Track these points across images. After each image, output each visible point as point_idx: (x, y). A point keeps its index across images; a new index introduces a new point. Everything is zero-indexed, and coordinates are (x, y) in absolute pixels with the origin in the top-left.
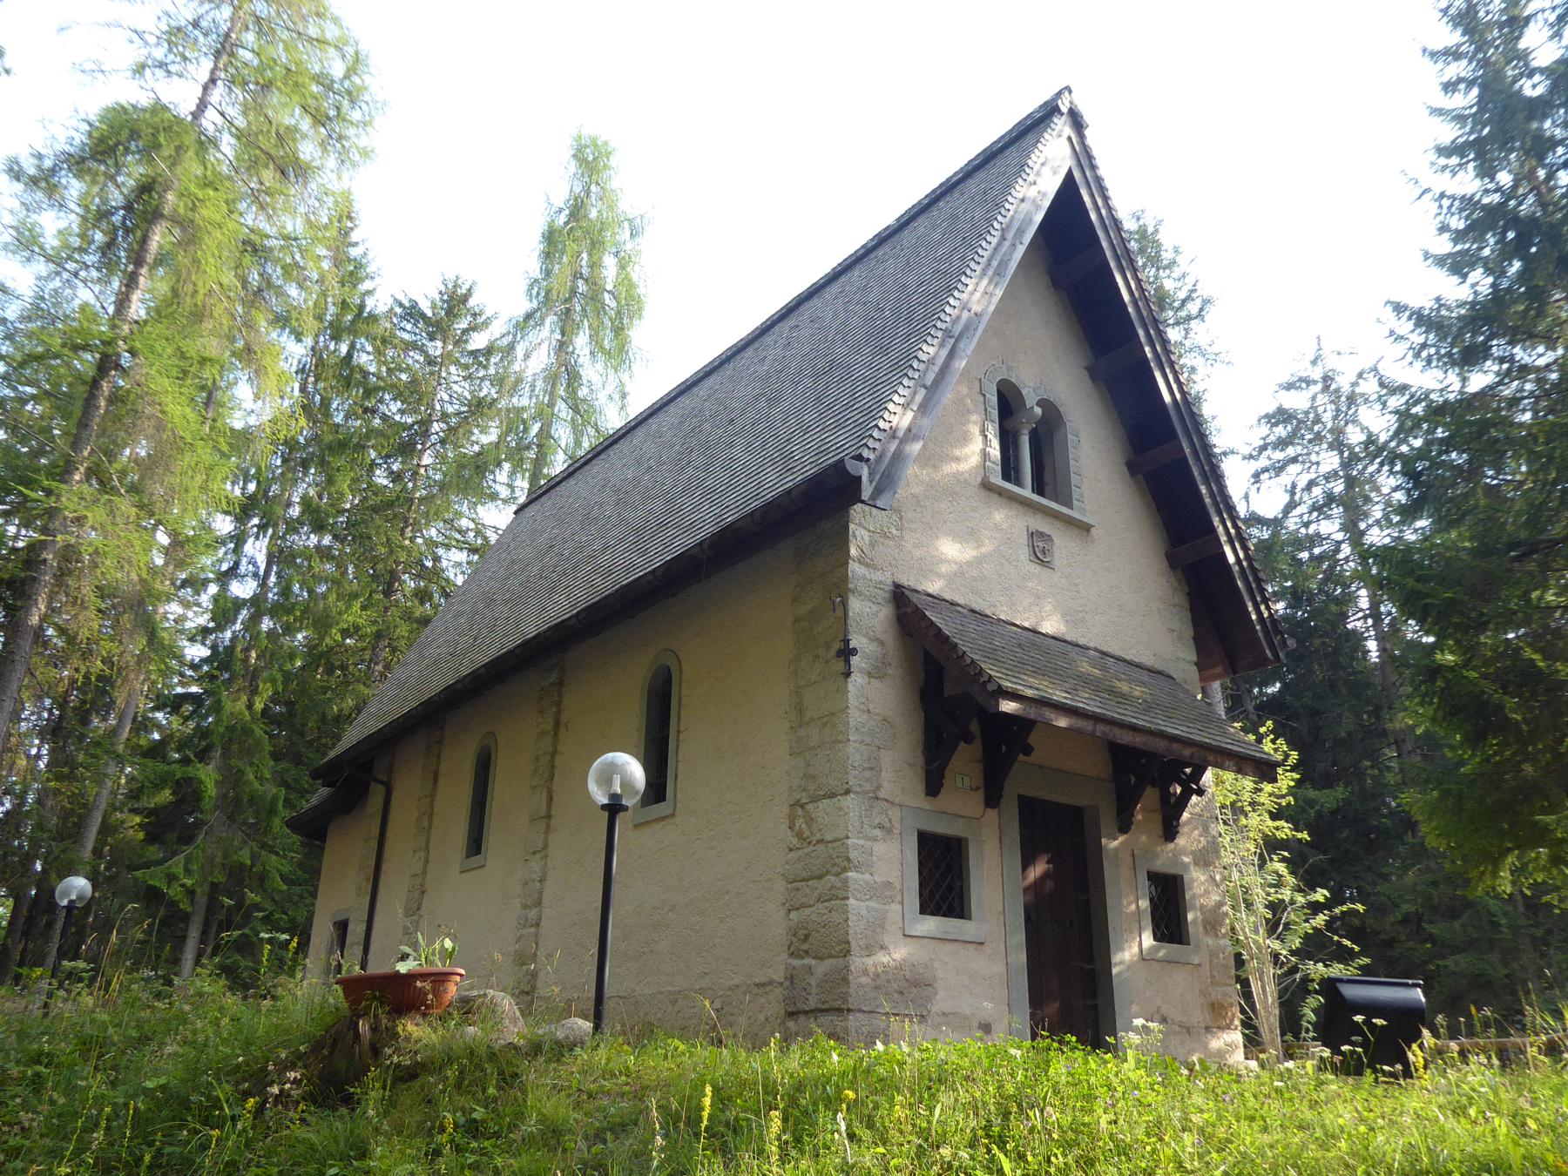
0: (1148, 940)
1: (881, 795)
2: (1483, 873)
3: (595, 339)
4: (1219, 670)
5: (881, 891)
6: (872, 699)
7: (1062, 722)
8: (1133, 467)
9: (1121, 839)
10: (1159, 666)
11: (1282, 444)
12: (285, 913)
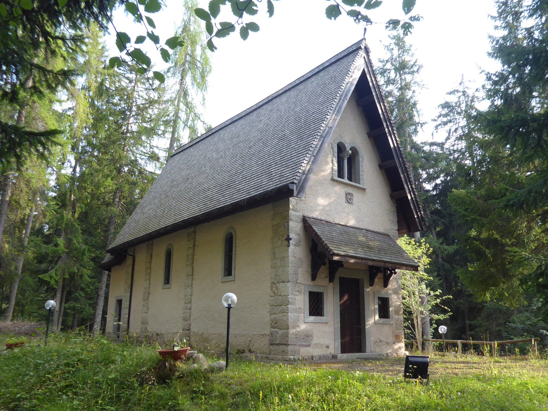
0: (377, 317)
1: (298, 282)
2: (481, 295)
3: (194, 78)
4: (405, 231)
6: (296, 253)
7: (352, 261)
8: (381, 167)
9: (370, 288)
10: (386, 232)
11: (446, 115)
12: (89, 288)
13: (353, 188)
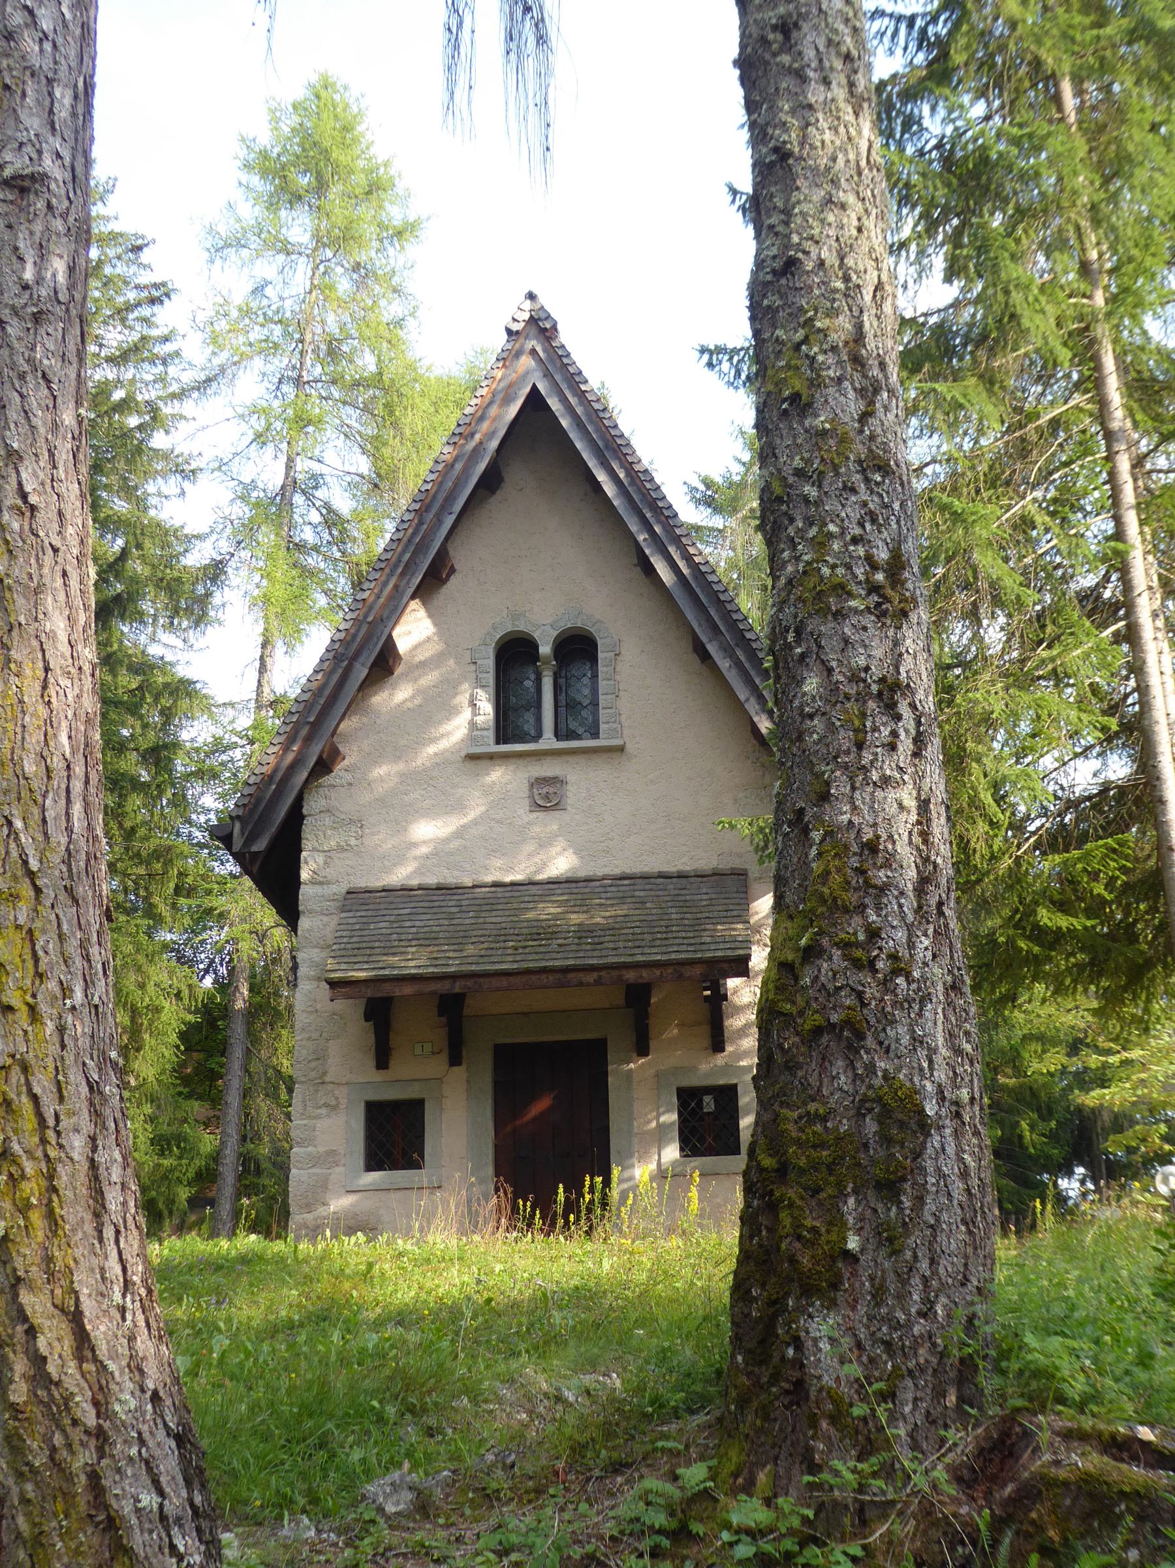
0: (671, 1153)
1: (327, 1079)
5: (330, 1158)
13: (604, 756)
